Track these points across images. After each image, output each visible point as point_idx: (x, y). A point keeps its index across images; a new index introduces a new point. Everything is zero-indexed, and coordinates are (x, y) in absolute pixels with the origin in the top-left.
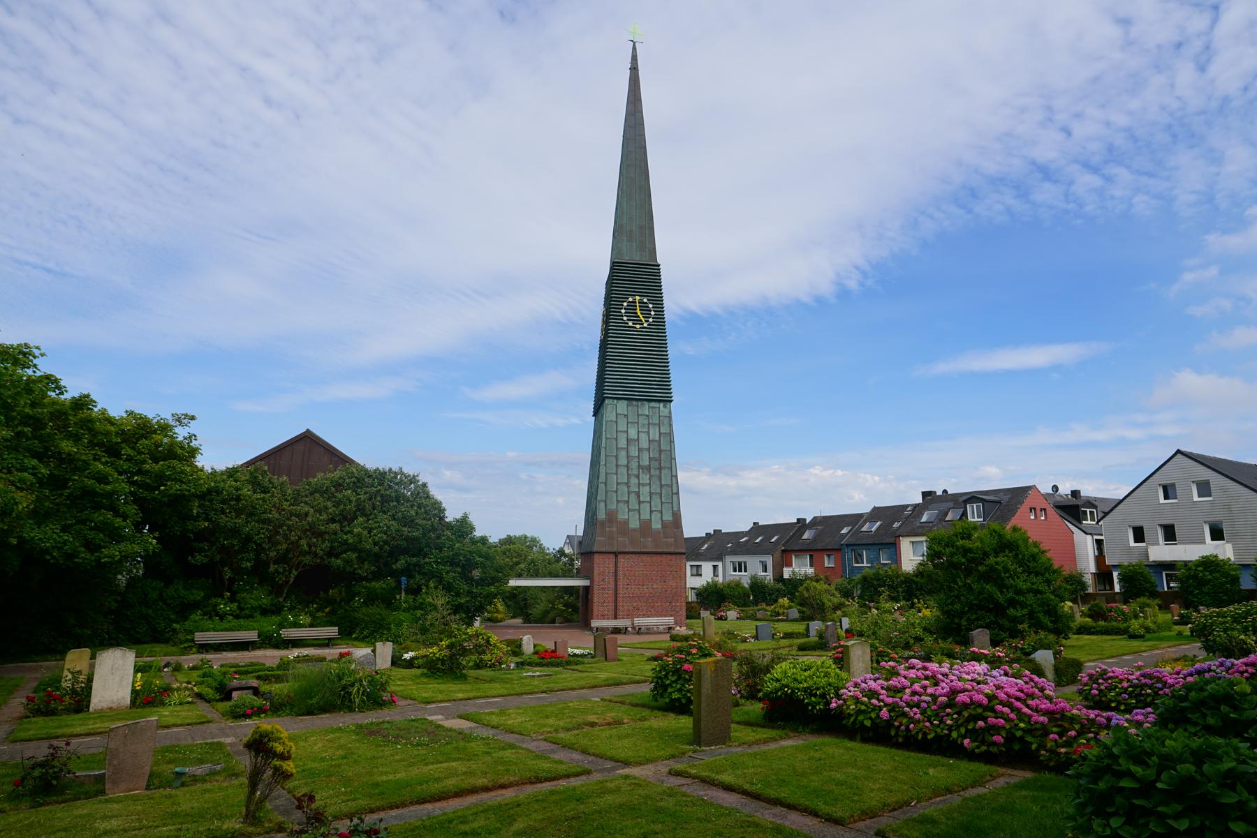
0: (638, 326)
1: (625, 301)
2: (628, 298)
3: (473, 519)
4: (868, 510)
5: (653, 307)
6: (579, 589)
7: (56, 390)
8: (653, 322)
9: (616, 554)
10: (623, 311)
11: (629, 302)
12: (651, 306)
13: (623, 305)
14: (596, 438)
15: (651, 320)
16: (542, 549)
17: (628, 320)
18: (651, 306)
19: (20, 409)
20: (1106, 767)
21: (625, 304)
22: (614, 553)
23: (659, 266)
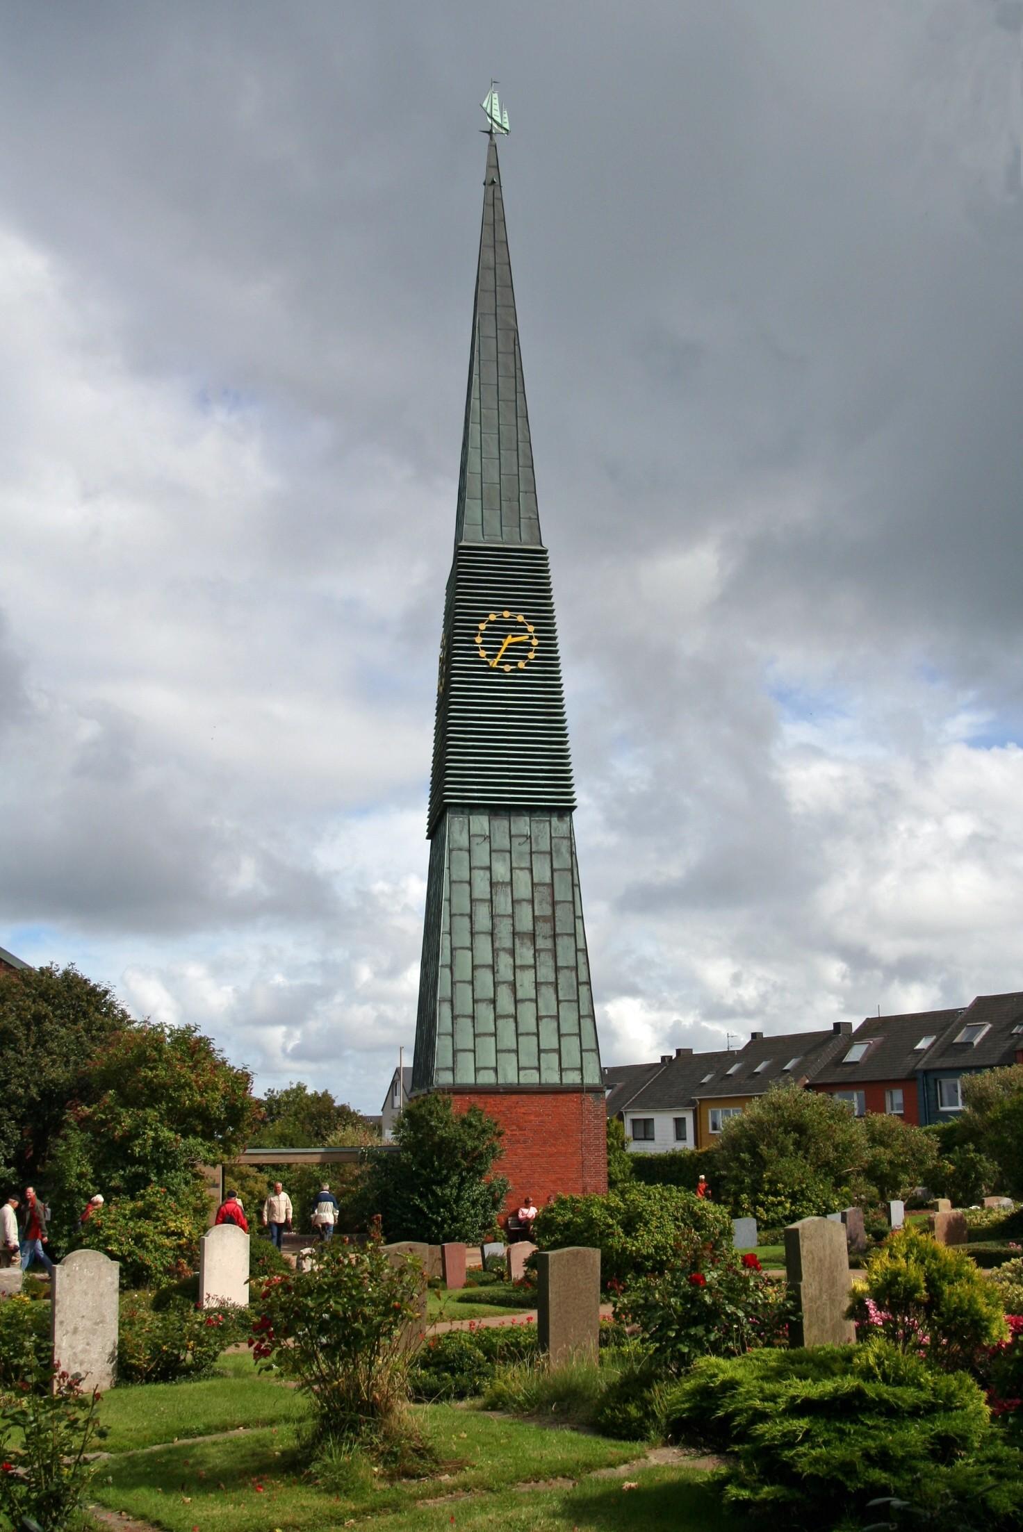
1: (482, 621)
2: (487, 615)
5: (536, 631)
11: (490, 622)
12: (531, 628)
13: (477, 629)
21: (482, 626)
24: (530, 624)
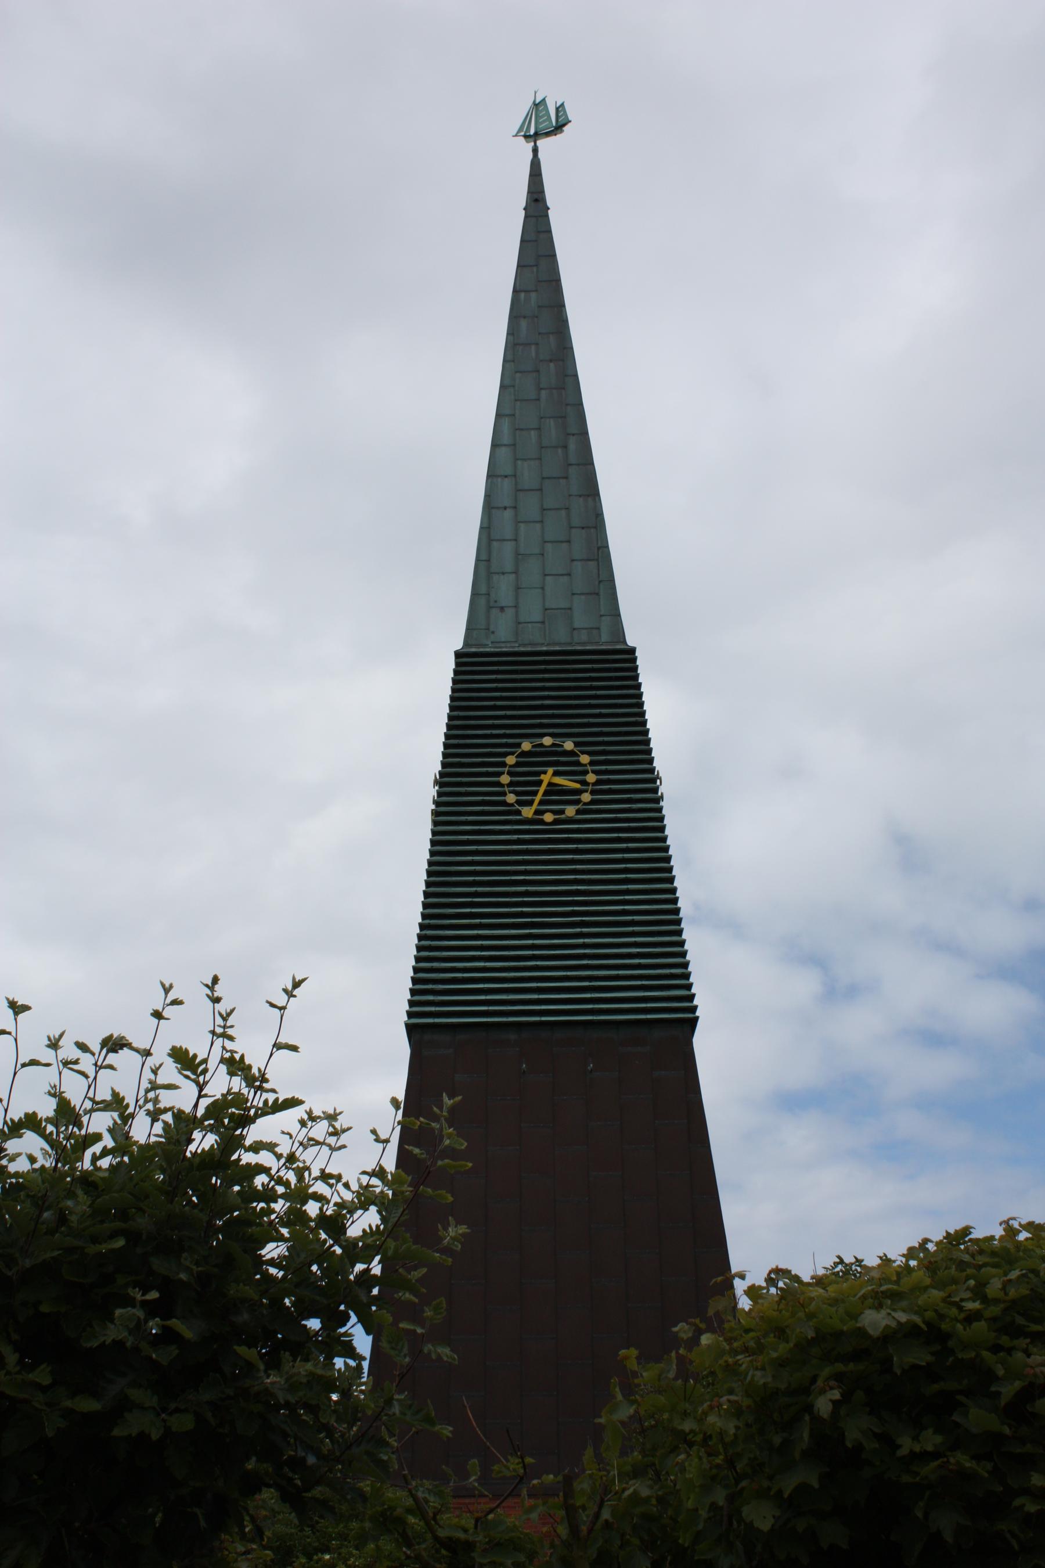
1: (512, 754)
3: (27, 1111)
4: (257, 1121)
5: (592, 763)
6: (712, 1317)
7: (48, 1132)
11: (524, 754)
12: (585, 759)
14: (518, 278)
15: (591, 778)
16: (228, 1069)
17: (518, 802)
18: (585, 759)
21: (511, 760)
24: (583, 753)
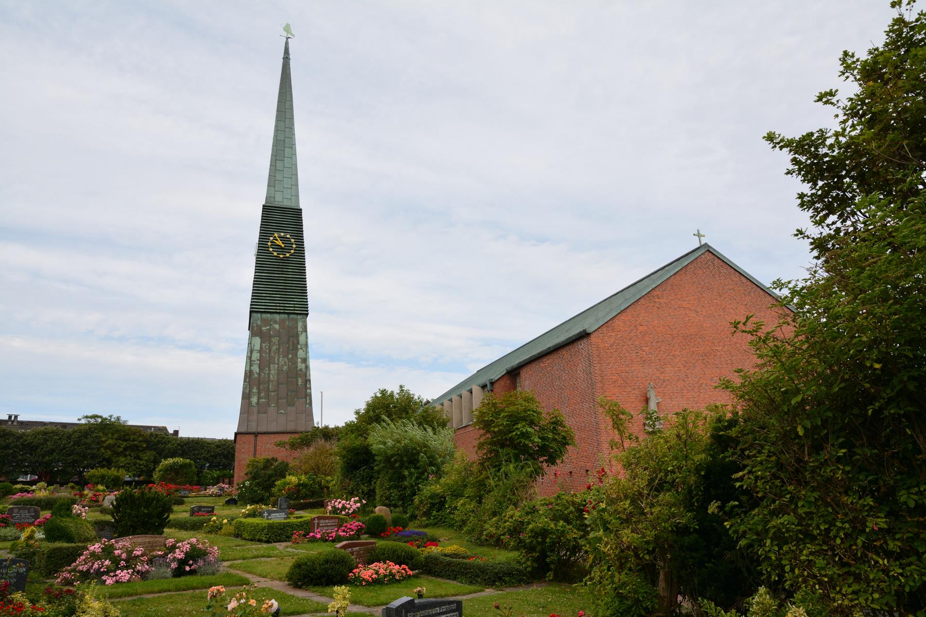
0: (281, 256)
8: (294, 253)
9: (256, 434)
10: (269, 244)
12: (293, 240)
15: (292, 251)
19: (805, 557)
20: (509, 530)
22: (253, 433)
23: (301, 210)
